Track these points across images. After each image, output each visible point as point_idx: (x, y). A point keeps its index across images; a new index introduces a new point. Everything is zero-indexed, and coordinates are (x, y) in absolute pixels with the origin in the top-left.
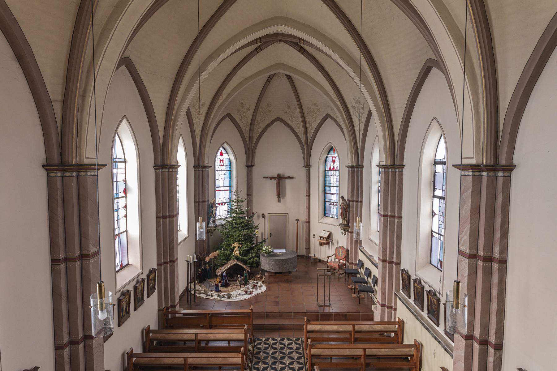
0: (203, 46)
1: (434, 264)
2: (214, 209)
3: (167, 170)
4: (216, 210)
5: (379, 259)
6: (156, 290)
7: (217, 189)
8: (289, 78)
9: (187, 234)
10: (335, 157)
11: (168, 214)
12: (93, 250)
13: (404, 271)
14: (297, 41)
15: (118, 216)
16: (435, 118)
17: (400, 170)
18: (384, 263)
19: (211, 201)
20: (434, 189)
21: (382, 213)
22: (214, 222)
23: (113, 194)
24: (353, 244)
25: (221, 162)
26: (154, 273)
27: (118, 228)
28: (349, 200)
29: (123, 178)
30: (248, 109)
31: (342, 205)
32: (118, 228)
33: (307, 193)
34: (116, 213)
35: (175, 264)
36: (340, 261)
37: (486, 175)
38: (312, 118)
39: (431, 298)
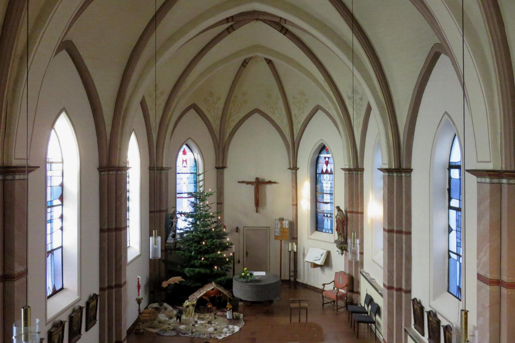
0: (160, 28)
1: (452, 293)
2: (174, 220)
3: (115, 173)
4: (176, 222)
5: (384, 285)
6: (98, 322)
7: (178, 196)
8: (269, 62)
9: (138, 252)
10: (329, 158)
11: (114, 227)
12: (18, 269)
13: (416, 301)
14: (278, 20)
15: (52, 228)
16: (446, 113)
17: (408, 175)
18: (390, 291)
19: (171, 211)
20: (450, 199)
21: (387, 228)
22: (174, 236)
23: (46, 202)
24: (352, 266)
25: (185, 162)
26: (96, 300)
27: (51, 243)
28: (346, 211)
29: (60, 182)
30: (219, 99)
31: (337, 217)
32: (51, 243)
33: (293, 201)
34: (49, 225)
35: (123, 288)
36: (338, 290)
37: (507, 183)
38: (299, 111)
39: (448, 335)
